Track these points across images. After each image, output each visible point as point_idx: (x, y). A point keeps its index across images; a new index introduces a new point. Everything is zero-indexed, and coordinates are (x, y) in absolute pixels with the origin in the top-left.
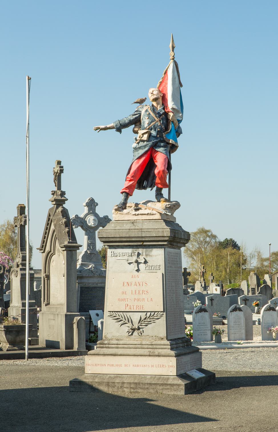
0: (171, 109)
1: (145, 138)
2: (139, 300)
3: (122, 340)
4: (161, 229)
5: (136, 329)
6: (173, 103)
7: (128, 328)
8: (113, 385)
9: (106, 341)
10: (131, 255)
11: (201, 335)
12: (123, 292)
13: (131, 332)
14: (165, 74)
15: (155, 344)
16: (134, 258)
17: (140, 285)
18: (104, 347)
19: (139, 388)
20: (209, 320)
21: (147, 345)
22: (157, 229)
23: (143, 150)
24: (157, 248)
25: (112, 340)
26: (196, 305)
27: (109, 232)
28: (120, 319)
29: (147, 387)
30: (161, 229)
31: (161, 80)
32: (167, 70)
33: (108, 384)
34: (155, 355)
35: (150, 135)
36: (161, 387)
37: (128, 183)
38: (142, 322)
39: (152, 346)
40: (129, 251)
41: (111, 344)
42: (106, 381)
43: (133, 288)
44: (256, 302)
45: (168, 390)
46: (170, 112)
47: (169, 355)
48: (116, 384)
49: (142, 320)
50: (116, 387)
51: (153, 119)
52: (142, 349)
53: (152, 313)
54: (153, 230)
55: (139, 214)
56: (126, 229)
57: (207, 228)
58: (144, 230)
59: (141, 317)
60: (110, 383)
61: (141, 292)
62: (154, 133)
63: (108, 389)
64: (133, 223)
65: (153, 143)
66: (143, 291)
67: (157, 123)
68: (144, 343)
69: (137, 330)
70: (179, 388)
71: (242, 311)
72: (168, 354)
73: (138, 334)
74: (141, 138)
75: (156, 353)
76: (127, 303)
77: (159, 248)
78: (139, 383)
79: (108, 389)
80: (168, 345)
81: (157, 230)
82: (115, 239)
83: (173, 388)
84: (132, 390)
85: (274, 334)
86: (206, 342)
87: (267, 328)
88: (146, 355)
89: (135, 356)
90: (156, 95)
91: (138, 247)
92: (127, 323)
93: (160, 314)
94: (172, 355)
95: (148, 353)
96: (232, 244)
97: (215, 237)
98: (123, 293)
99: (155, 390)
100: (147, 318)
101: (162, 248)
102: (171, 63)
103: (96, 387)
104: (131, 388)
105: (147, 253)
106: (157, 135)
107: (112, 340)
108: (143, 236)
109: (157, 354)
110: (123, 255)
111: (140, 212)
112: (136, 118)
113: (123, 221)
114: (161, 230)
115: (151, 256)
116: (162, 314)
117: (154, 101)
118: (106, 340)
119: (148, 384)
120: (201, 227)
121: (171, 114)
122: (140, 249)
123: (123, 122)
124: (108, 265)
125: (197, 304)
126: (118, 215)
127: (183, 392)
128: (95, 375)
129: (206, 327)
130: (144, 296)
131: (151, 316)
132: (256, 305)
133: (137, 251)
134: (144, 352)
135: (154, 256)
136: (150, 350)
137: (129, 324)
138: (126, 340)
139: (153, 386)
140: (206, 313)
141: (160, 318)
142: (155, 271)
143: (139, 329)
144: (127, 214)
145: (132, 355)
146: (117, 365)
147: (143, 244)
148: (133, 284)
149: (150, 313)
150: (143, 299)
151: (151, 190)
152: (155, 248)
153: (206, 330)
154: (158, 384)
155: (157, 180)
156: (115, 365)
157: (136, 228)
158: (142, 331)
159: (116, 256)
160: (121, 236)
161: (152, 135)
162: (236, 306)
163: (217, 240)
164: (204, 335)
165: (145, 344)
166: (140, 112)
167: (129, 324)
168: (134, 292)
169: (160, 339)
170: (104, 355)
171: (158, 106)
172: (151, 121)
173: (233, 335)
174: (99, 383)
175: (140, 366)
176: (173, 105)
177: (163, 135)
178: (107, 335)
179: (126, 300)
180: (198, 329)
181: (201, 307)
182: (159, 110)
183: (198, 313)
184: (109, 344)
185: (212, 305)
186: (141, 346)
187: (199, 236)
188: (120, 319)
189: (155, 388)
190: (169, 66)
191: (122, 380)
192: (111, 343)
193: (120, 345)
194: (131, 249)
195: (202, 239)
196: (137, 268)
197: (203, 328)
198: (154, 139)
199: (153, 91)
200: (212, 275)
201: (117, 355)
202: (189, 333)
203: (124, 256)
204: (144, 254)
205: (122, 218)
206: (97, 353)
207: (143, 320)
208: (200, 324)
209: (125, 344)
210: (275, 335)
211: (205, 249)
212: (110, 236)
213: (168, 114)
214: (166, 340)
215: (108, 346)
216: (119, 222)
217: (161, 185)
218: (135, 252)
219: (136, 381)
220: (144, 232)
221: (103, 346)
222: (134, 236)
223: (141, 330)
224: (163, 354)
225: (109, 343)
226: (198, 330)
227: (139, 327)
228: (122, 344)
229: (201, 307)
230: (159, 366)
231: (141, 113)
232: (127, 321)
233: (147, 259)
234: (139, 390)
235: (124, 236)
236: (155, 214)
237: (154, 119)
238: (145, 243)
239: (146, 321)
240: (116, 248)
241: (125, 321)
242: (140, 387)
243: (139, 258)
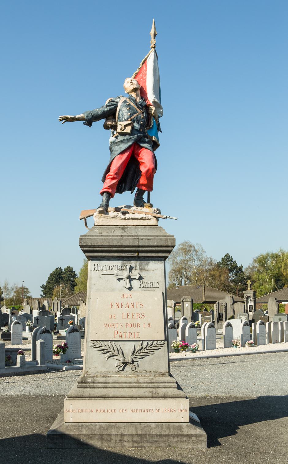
0: (152, 102)
1: (128, 130)
2: (133, 325)
3: (110, 377)
4: (163, 236)
5: (128, 363)
6: (154, 96)
7: (119, 362)
8: (108, 438)
9: (89, 378)
10: (121, 269)
11: (73, 352)
12: (111, 316)
13: (121, 366)
14: (143, 64)
15: (157, 382)
16: (126, 273)
17: (133, 307)
18: (88, 386)
19: (145, 442)
21: (146, 383)
22: (158, 236)
23: (126, 144)
24: (155, 260)
25: (96, 377)
26: (27, 324)
27: (95, 239)
28: (107, 349)
29: (155, 440)
30: (163, 236)
31: (137, 72)
32: (146, 60)
33: (102, 437)
34: (159, 396)
35: (133, 128)
36: (175, 440)
37: (111, 181)
38: (137, 354)
39: (153, 384)
40: (118, 264)
41: (96, 383)
42: (97, 433)
43: (125, 310)
45: (185, 443)
46: (152, 106)
47: (179, 396)
48: (113, 437)
49: (136, 352)
50: (112, 441)
51: (135, 111)
52: (139, 389)
53: (150, 343)
54: (153, 238)
55: (130, 218)
56: (117, 236)
58: (142, 237)
59: (134, 347)
60: (105, 436)
61: (135, 316)
62: (137, 126)
63: (102, 443)
64: (123, 229)
65: (138, 136)
66: (138, 315)
67: (140, 115)
68: (141, 381)
69: (131, 364)
70: (199, 439)
72: (177, 395)
73: (132, 369)
74: (123, 130)
75: (161, 394)
76: (116, 329)
77: (158, 260)
78: (145, 435)
79: (102, 443)
80: (174, 383)
81: (159, 238)
82: (102, 249)
83: (191, 440)
84: (136, 445)
86: (77, 359)
88: (147, 396)
89: (133, 399)
90: (136, 85)
91: (130, 259)
92: (117, 355)
93: (161, 343)
94: (183, 396)
95: (150, 394)
98: (111, 317)
99: (167, 443)
100: (143, 348)
101: (161, 261)
102: (151, 52)
103: (85, 442)
104: (134, 441)
105: (142, 267)
106: (140, 129)
107: (96, 377)
108: (140, 245)
109: (163, 395)
110: (110, 269)
111: (127, 216)
112: (111, 109)
113: (109, 227)
114: (163, 238)
115: (147, 270)
116: (162, 343)
117: (133, 92)
118: (89, 377)
119: (157, 435)
121: (153, 108)
122: (132, 262)
123: (95, 113)
124: (90, 281)
126: (102, 219)
127: (204, 445)
128: (80, 425)
129: (77, 345)
130: (139, 321)
131: (148, 346)
132: (71, 323)
133: (129, 264)
134: (145, 392)
135: (151, 270)
136: (151, 389)
137: (120, 357)
138: (116, 377)
139: (165, 439)
141: (160, 349)
142: (153, 289)
143: (133, 362)
144: (114, 217)
145: (129, 396)
146: (109, 411)
147: (139, 255)
148: (124, 305)
149: (147, 342)
150: (138, 324)
151: (132, 193)
152: (152, 260)
153: (78, 348)
154: (171, 435)
155: (143, 181)
156: (106, 411)
157: (129, 234)
158: (136, 365)
159: (101, 270)
160: (111, 244)
161: (135, 128)
164: (76, 352)
165: (143, 382)
166: (116, 102)
167: (120, 357)
168: (125, 316)
169: (160, 375)
170: (90, 397)
171: (137, 98)
172: (133, 112)
174: (90, 437)
175: (140, 411)
176: (154, 98)
177: (145, 129)
178: (89, 371)
179: (115, 325)
180: (71, 347)
181: (73, 328)
182: (139, 102)
183: (71, 333)
184: (94, 383)
186: (138, 385)
188: (107, 349)
189: (167, 441)
190: (149, 55)
191: (120, 432)
192: (97, 381)
193: (109, 384)
194: (121, 262)
196: (129, 286)
197: (75, 346)
198: (137, 132)
199: (131, 81)
200: (83, 301)
201: (108, 398)
202: (56, 351)
203: (111, 269)
204: (138, 267)
205: (108, 222)
206: (81, 395)
207: (137, 352)
208: (73, 343)
209: (116, 382)
212: (95, 244)
213: (148, 107)
214: (168, 376)
215: (93, 385)
216: (105, 228)
217: (146, 187)
218: (127, 266)
219: (140, 432)
220: (142, 239)
221: (86, 385)
222: (129, 245)
223: (136, 364)
224: (171, 394)
225: (94, 382)
227: (133, 360)
228: (112, 382)
229: (73, 328)
230: (167, 411)
231: (117, 104)
232: (116, 353)
233: (143, 274)
234: (145, 445)
235: (115, 245)
236: (151, 219)
237: (137, 110)
238: (140, 255)
239: (142, 352)
240: (100, 260)
241: (114, 352)
242: (146, 440)
243: (131, 273)
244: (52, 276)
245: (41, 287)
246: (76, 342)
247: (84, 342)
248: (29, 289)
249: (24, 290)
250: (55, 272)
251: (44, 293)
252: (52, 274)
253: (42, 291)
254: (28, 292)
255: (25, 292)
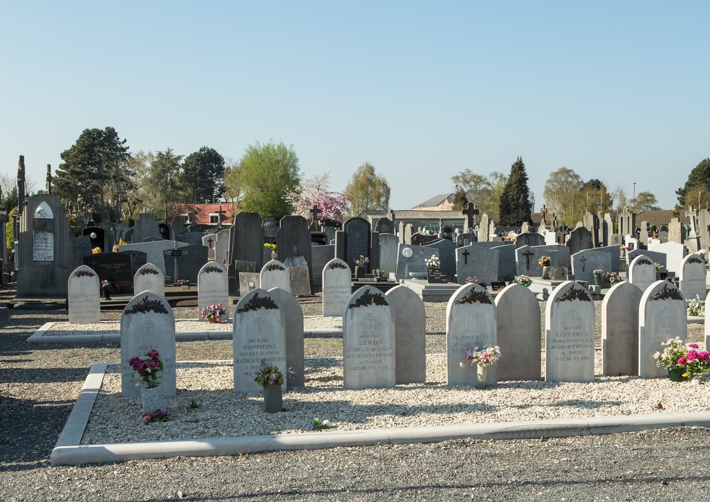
20: (283, 331)
44: (545, 258)
57: (568, 168)
71: (387, 305)
85: (480, 370)
87: (463, 351)
96: (596, 185)
97: (577, 177)
120: (563, 166)
125: (432, 262)
132: (544, 263)
140: (272, 311)
162: (368, 291)
163: (580, 180)
173: (357, 373)
180: (246, 357)
185: (466, 263)
187: (560, 176)
195: (563, 179)
200: (554, 216)
208: (252, 344)
210: (481, 373)
211: (567, 189)
226: (247, 361)
244: (695, 174)
245: (677, 192)
246: (266, 340)
247: (600, 306)
248: (655, 196)
249: (648, 198)
250: (702, 164)
251: (681, 202)
252: (694, 169)
253: (678, 198)
254: (653, 200)
255: (648, 201)
